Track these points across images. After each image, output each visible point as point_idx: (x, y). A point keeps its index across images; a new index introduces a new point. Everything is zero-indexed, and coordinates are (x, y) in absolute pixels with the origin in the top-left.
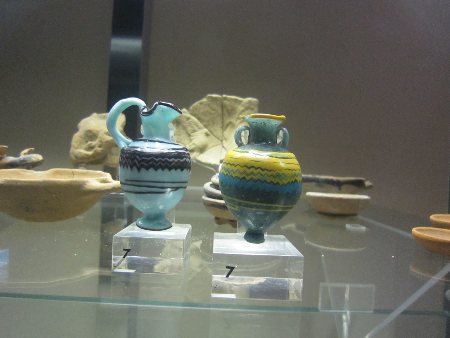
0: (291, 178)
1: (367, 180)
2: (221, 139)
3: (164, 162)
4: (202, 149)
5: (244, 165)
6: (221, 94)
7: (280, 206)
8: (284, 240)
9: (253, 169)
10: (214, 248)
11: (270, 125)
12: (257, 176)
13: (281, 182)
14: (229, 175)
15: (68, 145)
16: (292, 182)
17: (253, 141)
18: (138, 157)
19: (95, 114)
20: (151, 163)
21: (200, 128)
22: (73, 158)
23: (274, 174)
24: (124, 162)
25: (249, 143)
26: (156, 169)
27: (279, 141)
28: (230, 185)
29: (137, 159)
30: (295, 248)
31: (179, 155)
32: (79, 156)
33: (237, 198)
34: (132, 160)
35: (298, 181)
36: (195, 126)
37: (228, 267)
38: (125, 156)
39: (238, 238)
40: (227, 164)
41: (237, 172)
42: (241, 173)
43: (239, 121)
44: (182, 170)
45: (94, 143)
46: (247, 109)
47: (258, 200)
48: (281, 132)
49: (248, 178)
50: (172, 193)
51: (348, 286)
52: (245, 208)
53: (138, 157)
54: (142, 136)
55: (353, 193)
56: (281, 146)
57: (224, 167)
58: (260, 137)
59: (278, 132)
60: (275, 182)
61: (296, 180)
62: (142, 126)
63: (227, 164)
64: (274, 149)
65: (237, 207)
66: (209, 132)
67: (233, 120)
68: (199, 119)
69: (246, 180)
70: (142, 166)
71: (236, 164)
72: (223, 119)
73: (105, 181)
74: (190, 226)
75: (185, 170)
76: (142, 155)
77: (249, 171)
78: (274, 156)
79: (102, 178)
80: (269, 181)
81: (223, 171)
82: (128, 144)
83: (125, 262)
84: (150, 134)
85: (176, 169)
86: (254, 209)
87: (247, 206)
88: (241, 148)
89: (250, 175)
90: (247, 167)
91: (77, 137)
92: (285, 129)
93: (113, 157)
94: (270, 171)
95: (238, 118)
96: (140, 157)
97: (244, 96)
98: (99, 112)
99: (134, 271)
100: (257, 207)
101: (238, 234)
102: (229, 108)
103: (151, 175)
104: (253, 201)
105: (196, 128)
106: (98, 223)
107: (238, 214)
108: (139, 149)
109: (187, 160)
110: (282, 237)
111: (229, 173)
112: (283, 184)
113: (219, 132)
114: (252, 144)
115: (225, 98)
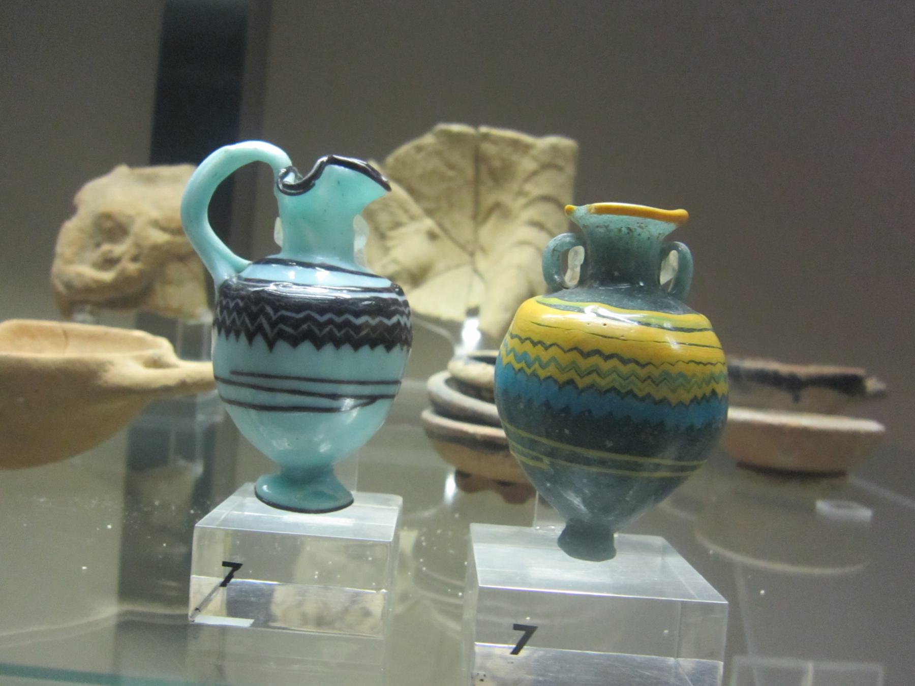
0: (700, 387)
1: (869, 375)
2: (472, 250)
3: (340, 327)
4: (418, 276)
5: (570, 347)
6: (475, 123)
7: (664, 462)
8: (663, 552)
9: (595, 360)
10: (478, 569)
11: (645, 235)
12: (608, 379)
13: (673, 398)
14: (529, 371)
15: (47, 253)
16: (704, 396)
17: (594, 277)
18: (269, 310)
19: (122, 171)
20: (305, 327)
21: (413, 218)
22: (61, 288)
23: (656, 373)
24: (228, 322)
25: (582, 282)
26: (319, 344)
27: (665, 277)
28: (530, 402)
29: (267, 316)
30: (701, 577)
31: (381, 308)
32: (77, 283)
33: (548, 436)
34: (253, 317)
35: (720, 395)
36: (399, 212)
37: (517, 627)
38: (232, 305)
39: (539, 541)
40: (522, 341)
41: (553, 364)
42: (561, 369)
43: (522, 201)
44: (389, 347)
45: (119, 249)
46: (546, 166)
47: (609, 444)
48: (673, 256)
49: (581, 383)
50: (355, 413)
51: (810, 667)
52: (569, 464)
53: (269, 310)
54: (278, 249)
55: (830, 411)
56: (670, 294)
57: (513, 350)
58: (615, 268)
59: (664, 253)
60: (658, 397)
61: (714, 392)
62: (278, 223)
63: (522, 341)
64: (655, 303)
65: (547, 460)
66: (437, 230)
67: (505, 198)
68: (411, 191)
69: (576, 388)
70: (281, 335)
71: (548, 343)
72: (477, 194)
73: (156, 363)
74: (399, 500)
75: (396, 350)
76: (279, 303)
77: (585, 364)
78: (653, 321)
79: (149, 353)
80: (640, 394)
81: (511, 358)
82: (239, 270)
83: (220, 597)
84: (302, 246)
85: (373, 344)
86: (594, 470)
87: (573, 459)
88: (562, 298)
89: (589, 373)
90: (581, 352)
91: (71, 230)
92: (683, 246)
93: (170, 290)
94: (643, 366)
95: (520, 193)
96: (276, 310)
97: (539, 132)
98: (133, 163)
99: (251, 621)
100: (602, 463)
101: (537, 529)
102: (497, 164)
103: (305, 360)
104: (592, 447)
105: (403, 218)
106: (120, 468)
107: (548, 480)
108: (271, 288)
109: (403, 320)
110: (658, 541)
111: (529, 366)
112: (681, 403)
113: (465, 231)
114: (591, 287)
115: (486, 137)
